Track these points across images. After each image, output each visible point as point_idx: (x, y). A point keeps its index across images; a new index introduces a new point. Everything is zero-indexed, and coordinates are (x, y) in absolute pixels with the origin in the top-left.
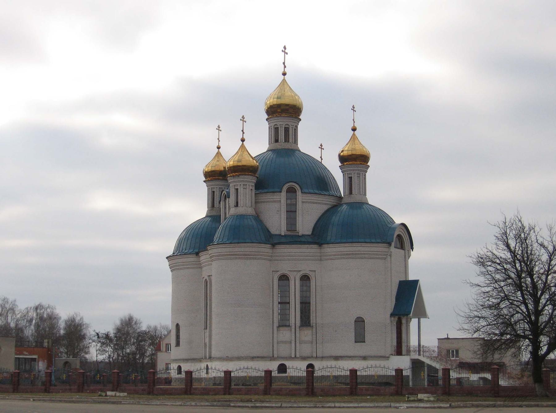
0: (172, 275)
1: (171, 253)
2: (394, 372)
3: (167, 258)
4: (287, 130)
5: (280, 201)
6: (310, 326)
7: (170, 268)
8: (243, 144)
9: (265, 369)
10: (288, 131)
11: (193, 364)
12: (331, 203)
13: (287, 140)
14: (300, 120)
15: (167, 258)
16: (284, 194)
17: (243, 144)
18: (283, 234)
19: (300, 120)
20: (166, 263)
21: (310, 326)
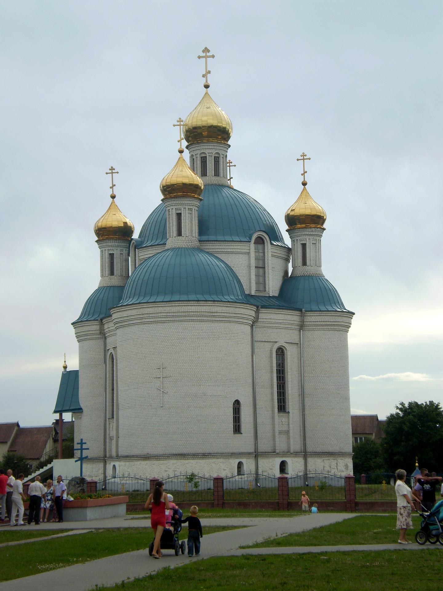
0: (80, 347)
1: (76, 318)
2: (343, 481)
3: (72, 324)
4: (217, 161)
5: (249, 253)
6: (285, 412)
7: (77, 337)
8: (304, 187)
9: (151, 478)
10: (218, 162)
11: (127, 463)
12: (200, 255)
13: (217, 174)
14: (229, 146)
15: (72, 324)
16: (252, 245)
17: (304, 187)
18: (253, 293)
19: (229, 146)
20: (72, 330)
21: (285, 412)
